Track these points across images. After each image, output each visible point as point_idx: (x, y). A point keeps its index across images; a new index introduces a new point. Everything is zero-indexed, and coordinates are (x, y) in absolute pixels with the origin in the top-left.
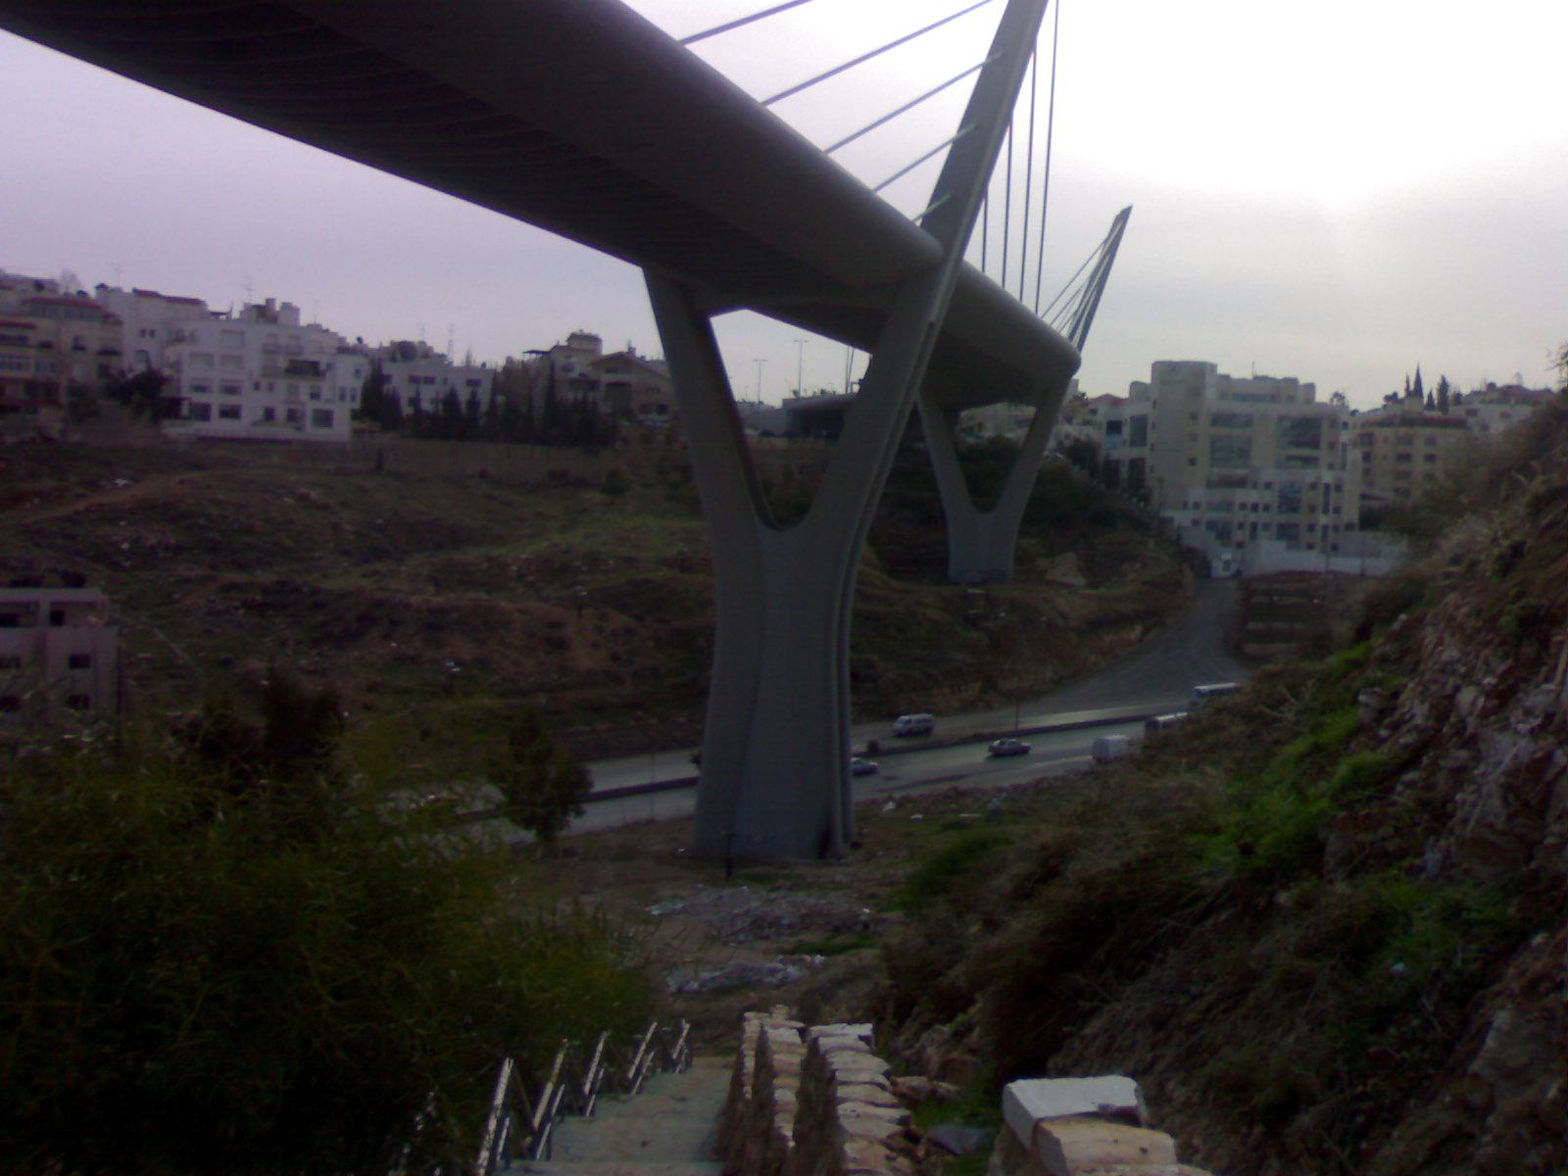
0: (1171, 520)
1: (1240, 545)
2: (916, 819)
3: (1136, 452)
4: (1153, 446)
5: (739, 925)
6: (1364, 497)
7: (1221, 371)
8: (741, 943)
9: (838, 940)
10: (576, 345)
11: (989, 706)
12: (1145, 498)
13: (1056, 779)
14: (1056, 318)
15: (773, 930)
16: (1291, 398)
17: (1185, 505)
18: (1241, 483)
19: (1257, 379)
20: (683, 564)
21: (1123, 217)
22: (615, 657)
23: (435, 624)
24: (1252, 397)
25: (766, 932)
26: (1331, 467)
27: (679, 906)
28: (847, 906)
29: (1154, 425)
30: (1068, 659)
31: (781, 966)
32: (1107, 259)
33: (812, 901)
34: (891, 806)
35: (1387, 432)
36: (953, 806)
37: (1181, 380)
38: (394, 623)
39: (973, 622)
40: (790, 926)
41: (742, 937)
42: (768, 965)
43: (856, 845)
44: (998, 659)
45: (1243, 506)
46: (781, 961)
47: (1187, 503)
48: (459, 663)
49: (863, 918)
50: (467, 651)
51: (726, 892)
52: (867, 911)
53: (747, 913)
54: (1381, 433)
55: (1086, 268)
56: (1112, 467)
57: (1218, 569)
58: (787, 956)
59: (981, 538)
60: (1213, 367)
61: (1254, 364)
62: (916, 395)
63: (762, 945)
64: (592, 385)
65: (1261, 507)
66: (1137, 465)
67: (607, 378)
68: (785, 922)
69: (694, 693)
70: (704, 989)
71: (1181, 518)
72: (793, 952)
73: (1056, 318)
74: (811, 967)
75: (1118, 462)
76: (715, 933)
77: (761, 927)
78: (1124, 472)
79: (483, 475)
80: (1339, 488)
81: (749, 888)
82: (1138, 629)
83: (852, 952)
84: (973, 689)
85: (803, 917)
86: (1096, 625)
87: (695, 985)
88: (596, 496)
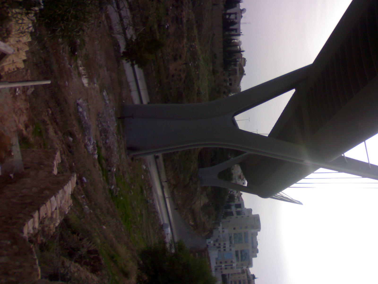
0: (220, 226)
1: (214, 245)
2: (142, 177)
3: (235, 213)
4: (237, 217)
5: (104, 124)
6: (229, 275)
7: (258, 233)
8: (98, 125)
9: (103, 161)
10: (243, 60)
11: (169, 187)
12: (224, 218)
13: (158, 217)
14: (286, 194)
15: (104, 137)
16: (253, 252)
17: (223, 228)
18: (231, 243)
19: (257, 242)
20: (199, 93)
21: (300, 203)
22: (173, 76)
23: (177, 20)
24: (252, 242)
25: (103, 134)
26: (237, 265)
27: (108, 102)
28: (115, 161)
29: (242, 217)
30: (182, 206)
31: (92, 143)
32: (279, 198)
33: (115, 149)
34: (145, 167)
35: (246, 277)
36: (147, 188)
37: (255, 223)
38: (177, 7)
39: (191, 179)
40: (106, 143)
41: (100, 126)
42: (92, 138)
43: (132, 159)
44: (181, 188)
45: (225, 244)
46: (94, 142)
47: (224, 230)
48: (168, 28)
49: (112, 169)
50: (171, 30)
51: (114, 118)
52: (115, 170)
53: (109, 126)
54: (245, 274)
55: (283, 194)
56: (229, 207)
57: (208, 241)
58: (96, 144)
59: (210, 176)
60: (259, 231)
61: (259, 240)
62: (248, 152)
63: (98, 134)
64: (235, 65)
65: (225, 248)
66: (231, 214)
67: (237, 68)
68: (107, 141)
69: (166, 100)
70: (79, 114)
71: (220, 228)
72: (97, 146)
73: (286, 194)
74: (93, 154)
75: (231, 208)
76: (100, 115)
77: (104, 132)
78: (229, 210)
79: (214, 34)
80: (232, 268)
81: (116, 125)
82: (192, 224)
83: (100, 168)
84: (173, 182)
85: (110, 147)
86: (193, 212)
87: (81, 110)
88: (211, 68)
